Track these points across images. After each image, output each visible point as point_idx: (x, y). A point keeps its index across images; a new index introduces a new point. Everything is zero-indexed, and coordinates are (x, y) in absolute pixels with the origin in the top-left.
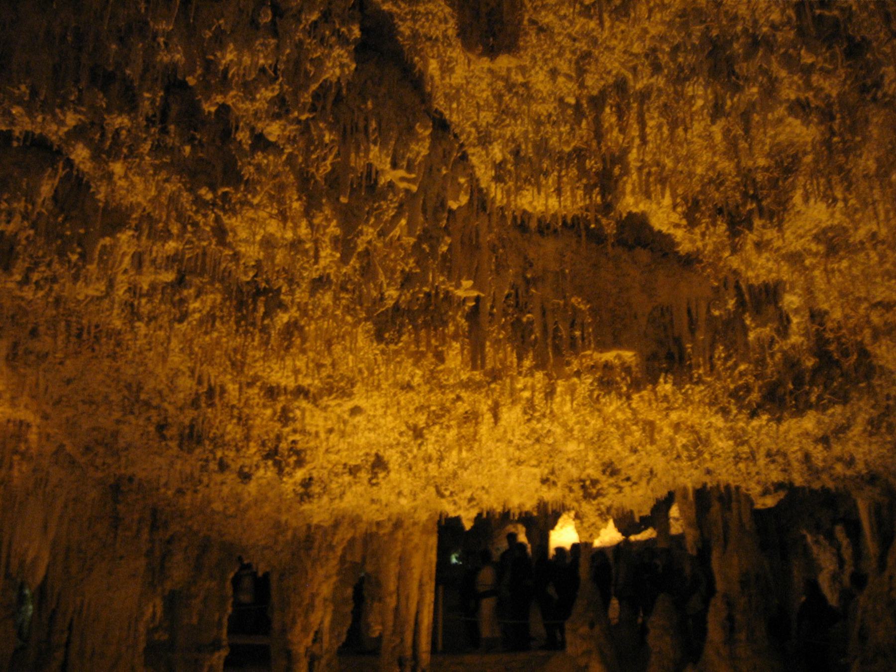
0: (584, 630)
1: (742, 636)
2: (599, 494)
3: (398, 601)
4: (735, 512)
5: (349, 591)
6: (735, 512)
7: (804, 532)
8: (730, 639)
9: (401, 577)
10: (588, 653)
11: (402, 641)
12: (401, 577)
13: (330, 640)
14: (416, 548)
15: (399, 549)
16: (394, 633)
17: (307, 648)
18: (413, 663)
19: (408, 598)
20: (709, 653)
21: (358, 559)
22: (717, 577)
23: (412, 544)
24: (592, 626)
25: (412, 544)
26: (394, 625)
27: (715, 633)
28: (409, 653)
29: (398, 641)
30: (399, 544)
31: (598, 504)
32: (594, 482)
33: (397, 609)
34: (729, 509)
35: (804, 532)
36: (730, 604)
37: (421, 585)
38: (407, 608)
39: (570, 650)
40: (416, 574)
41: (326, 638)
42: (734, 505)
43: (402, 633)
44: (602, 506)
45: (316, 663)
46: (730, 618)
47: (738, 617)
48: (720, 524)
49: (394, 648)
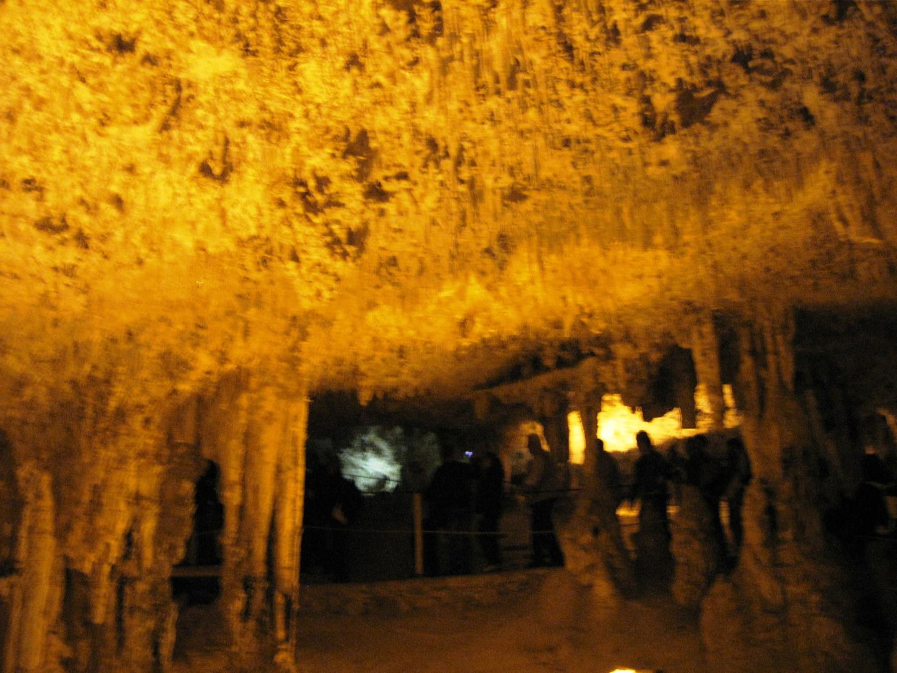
0: (586, 538)
1: (788, 535)
2: (334, 203)
3: (244, 496)
4: (772, 367)
5: (188, 487)
6: (772, 367)
7: (883, 412)
8: (772, 541)
9: (247, 462)
10: (591, 568)
11: (250, 553)
12: (247, 462)
13: (155, 555)
14: (270, 418)
15: (243, 421)
16: (238, 542)
17: (113, 567)
18: (267, 585)
19: (256, 490)
20: (746, 558)
21: (190, 439)
22: (753, 456)
23: (263, 413)
24: (596, 532)
25: (263, 413)
26: (240, 531)
27: (753, 534)
28: (260, 570)
29: (243, 553)
30: (242, 413)
31: (326, 225)
32: (322, 182)
33: (242, 508)
34: (765, 365)
35: (883, 412)
36: (770, 493)
37: (279, 471)
38: (256, 506)
39: (570, 565)
40: (269, 455)
41: (148, 553)
42: (771, 358)
43: (249, 541)
44: (335, 227)
45: (127, 590)
46: (771, 511)
47: (781, 508)
48: (753, 386)
49: (239, 564)
